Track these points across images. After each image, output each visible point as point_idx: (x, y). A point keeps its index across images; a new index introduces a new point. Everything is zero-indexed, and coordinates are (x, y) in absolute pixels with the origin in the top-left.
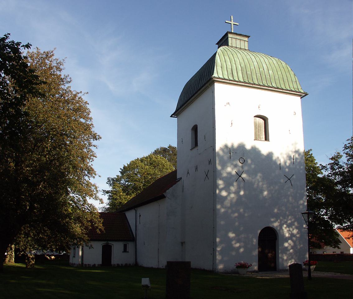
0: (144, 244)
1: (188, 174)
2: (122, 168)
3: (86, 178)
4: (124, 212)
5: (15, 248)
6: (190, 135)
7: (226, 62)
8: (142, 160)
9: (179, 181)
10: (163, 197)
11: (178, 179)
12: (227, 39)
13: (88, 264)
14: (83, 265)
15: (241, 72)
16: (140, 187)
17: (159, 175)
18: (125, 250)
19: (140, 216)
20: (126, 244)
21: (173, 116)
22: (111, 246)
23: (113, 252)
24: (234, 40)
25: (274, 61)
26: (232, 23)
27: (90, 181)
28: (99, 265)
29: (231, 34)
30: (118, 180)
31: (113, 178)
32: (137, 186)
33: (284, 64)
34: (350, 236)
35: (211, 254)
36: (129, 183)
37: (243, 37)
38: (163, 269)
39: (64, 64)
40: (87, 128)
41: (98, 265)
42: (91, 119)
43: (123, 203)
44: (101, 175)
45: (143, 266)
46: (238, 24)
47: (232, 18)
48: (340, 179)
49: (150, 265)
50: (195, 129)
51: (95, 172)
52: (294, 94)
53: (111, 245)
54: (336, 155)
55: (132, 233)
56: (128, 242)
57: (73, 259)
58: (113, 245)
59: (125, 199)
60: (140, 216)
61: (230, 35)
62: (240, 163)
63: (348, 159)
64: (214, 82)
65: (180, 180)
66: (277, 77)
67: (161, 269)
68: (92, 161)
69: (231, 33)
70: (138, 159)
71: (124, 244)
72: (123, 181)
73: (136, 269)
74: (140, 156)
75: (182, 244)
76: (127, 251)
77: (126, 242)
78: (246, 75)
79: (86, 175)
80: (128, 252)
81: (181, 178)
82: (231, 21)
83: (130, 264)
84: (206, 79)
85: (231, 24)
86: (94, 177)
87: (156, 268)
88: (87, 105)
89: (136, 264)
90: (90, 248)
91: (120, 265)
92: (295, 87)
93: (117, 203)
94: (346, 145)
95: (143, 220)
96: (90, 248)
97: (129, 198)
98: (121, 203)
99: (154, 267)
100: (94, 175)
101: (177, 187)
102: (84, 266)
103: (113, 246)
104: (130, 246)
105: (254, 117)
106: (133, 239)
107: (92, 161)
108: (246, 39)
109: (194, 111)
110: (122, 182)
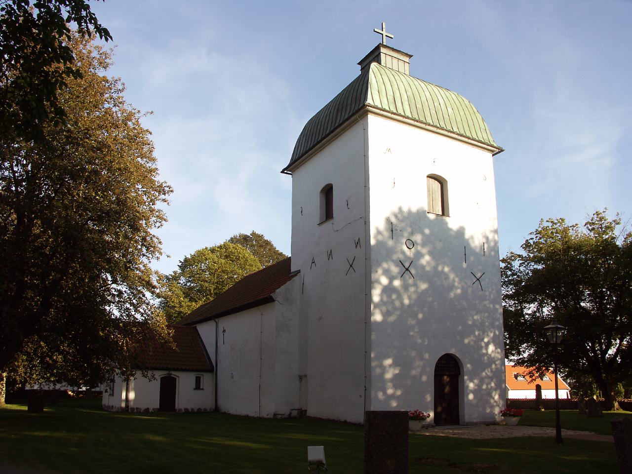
0: (232, 378)
1: (313, 264)
2: (183, 261)
3: (144, 260)
4: (195, 326)
5: (8, 378)
6: (318, 201)
7: (386, 85)
8: (213, 250)
9: (296, 275)
10: (271, 300)
11: (293, 272)
12: (377, 56)
13: (137, 408)
14: (128, 410)
15: (407, 103)
16: (210, 290)
17: (239, 274)
18: (198, 387)
19: (224, 331)
20: (200, 377)
21: (286, 171)
22: (176, 379)
23: (179, 393)
24: (389, 58)
25: (452, 95)
26: (384, 33)
27: (149, 265)
28: (155, 409)
29: (385, 48)
30: (175, 278)
31: (168, 275)
32: (207, 288)
33: (466, 102)
34: (525, 373)
35: (361, 396)
36: (192, 285)
37: (402, 55)
38: (270, 418)
39: (112, 57)
40: (146, 176)
41: (153, 409)
42: (154, 160)
43: (186, 313)
44: (170, 255)
45: (229, 412)
46: (393, 37)
47: (384, 26)
48: (514, 291)
49: (243, 412)
50: (328, 192)
51: (160, 249)
52: (484, 148)
53: (175, 377)
54: (509, 255)
55: (209, 357)
56: (204, 374)
57: (462, 425)
58: (179, 377)
59: (188, 307)
60: (224, 331)
61: (383, 50)
62: (408, 247)
63: (520, 264)
64: (368, 112)
65: (298, 273)
66: (459, 120)
67: (265, 418)
68: (159, 227)
69: (386, 47)
70: (206, 248)
71: (196, 377)
72: (183, 280)
73: (214, 416)
74: (210, 245)
75: (300, 378)
76: (201, 388)
77: (198, 373)
78: (415, 110)
79: (144, 255)
80: (203, 389)
81: (299, 272)
82: (382, 31)
83: (205, 409)
84: (316, 139)
85: (382, 34)
86: (158, 258)
87: (256, 416)
88: (149, 136)
89: (217, 410)
90: (150, 381)
91: (190, 411)
92: (485, 137)
93: (175, 313)
94: (527, 241)
95: (231, 339)
96: (150, 381)
97: (195, 306)
98: (180, 312)
99: (251, 414)
100: (157, 254)
101: (293, 285)
102: (130, 410)
103: (179, 379)
104: (207, 380)
105: (427, 177)
106: (211, 369)
107: (159, 227)
108: (407, 59)
109: (325, 166)
110: (182, 282)
